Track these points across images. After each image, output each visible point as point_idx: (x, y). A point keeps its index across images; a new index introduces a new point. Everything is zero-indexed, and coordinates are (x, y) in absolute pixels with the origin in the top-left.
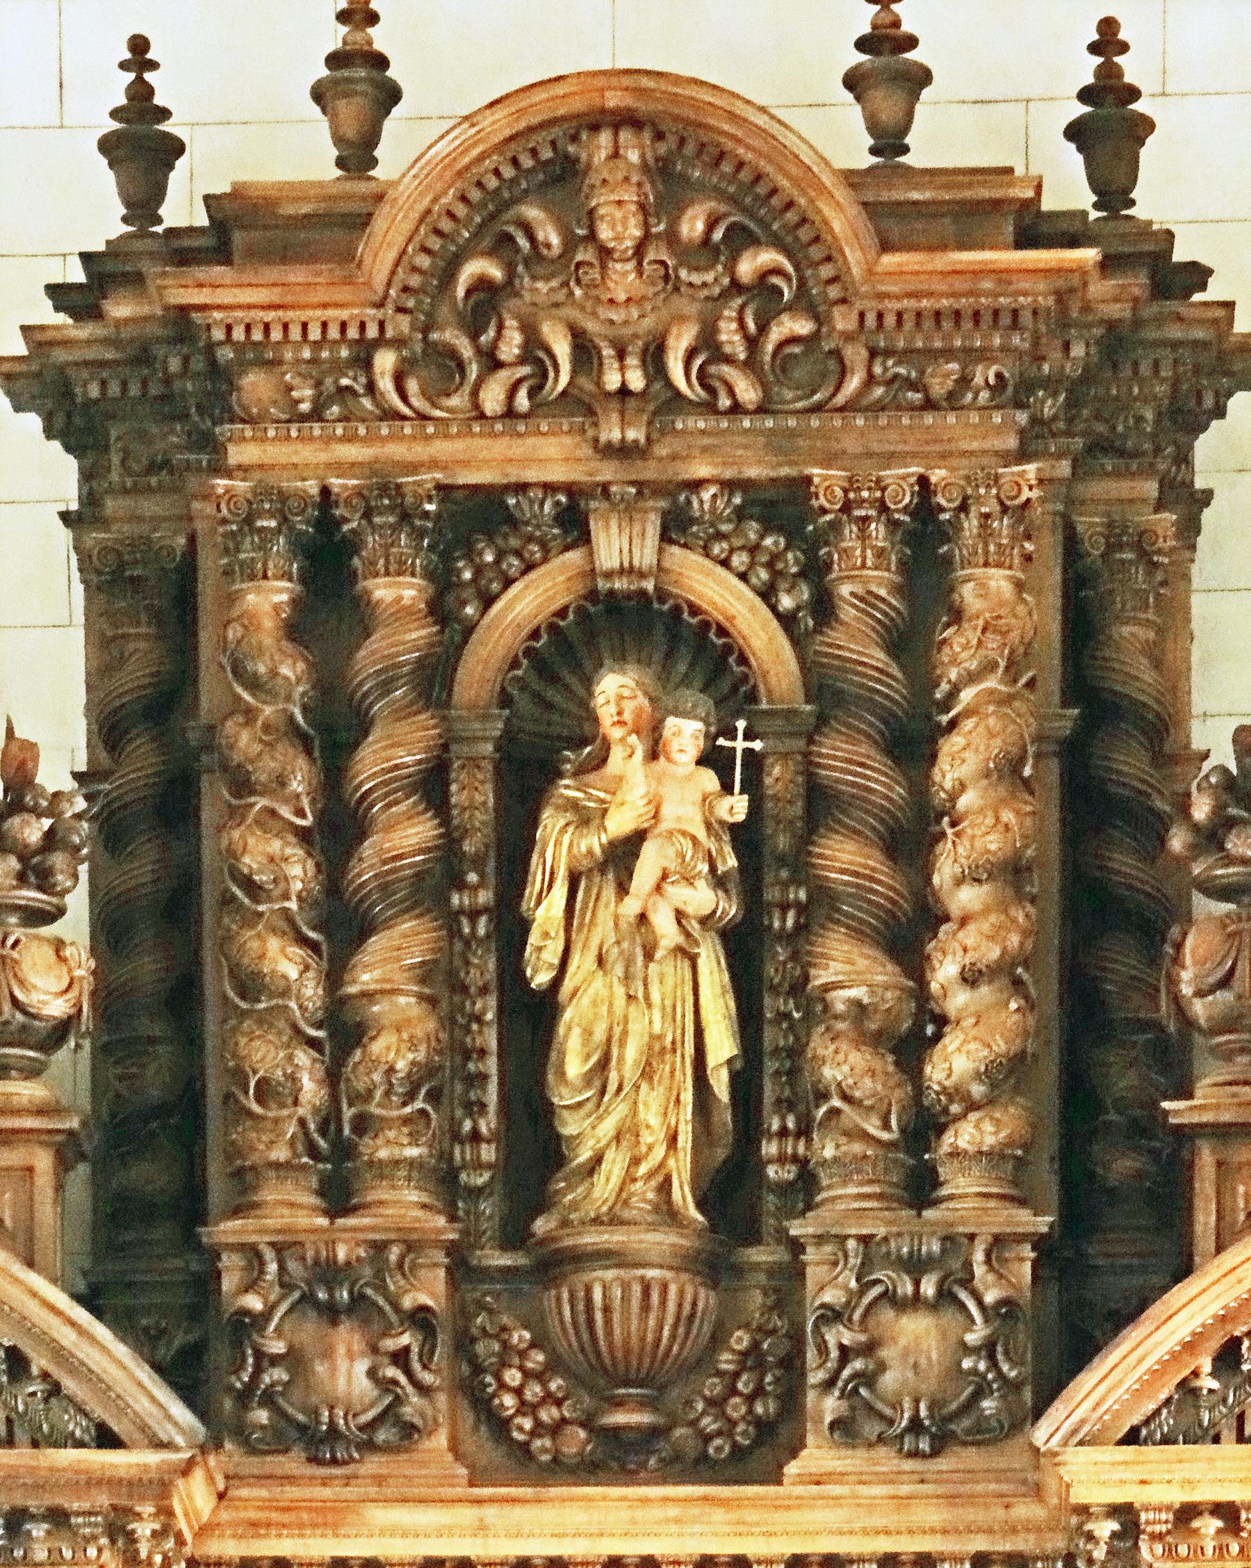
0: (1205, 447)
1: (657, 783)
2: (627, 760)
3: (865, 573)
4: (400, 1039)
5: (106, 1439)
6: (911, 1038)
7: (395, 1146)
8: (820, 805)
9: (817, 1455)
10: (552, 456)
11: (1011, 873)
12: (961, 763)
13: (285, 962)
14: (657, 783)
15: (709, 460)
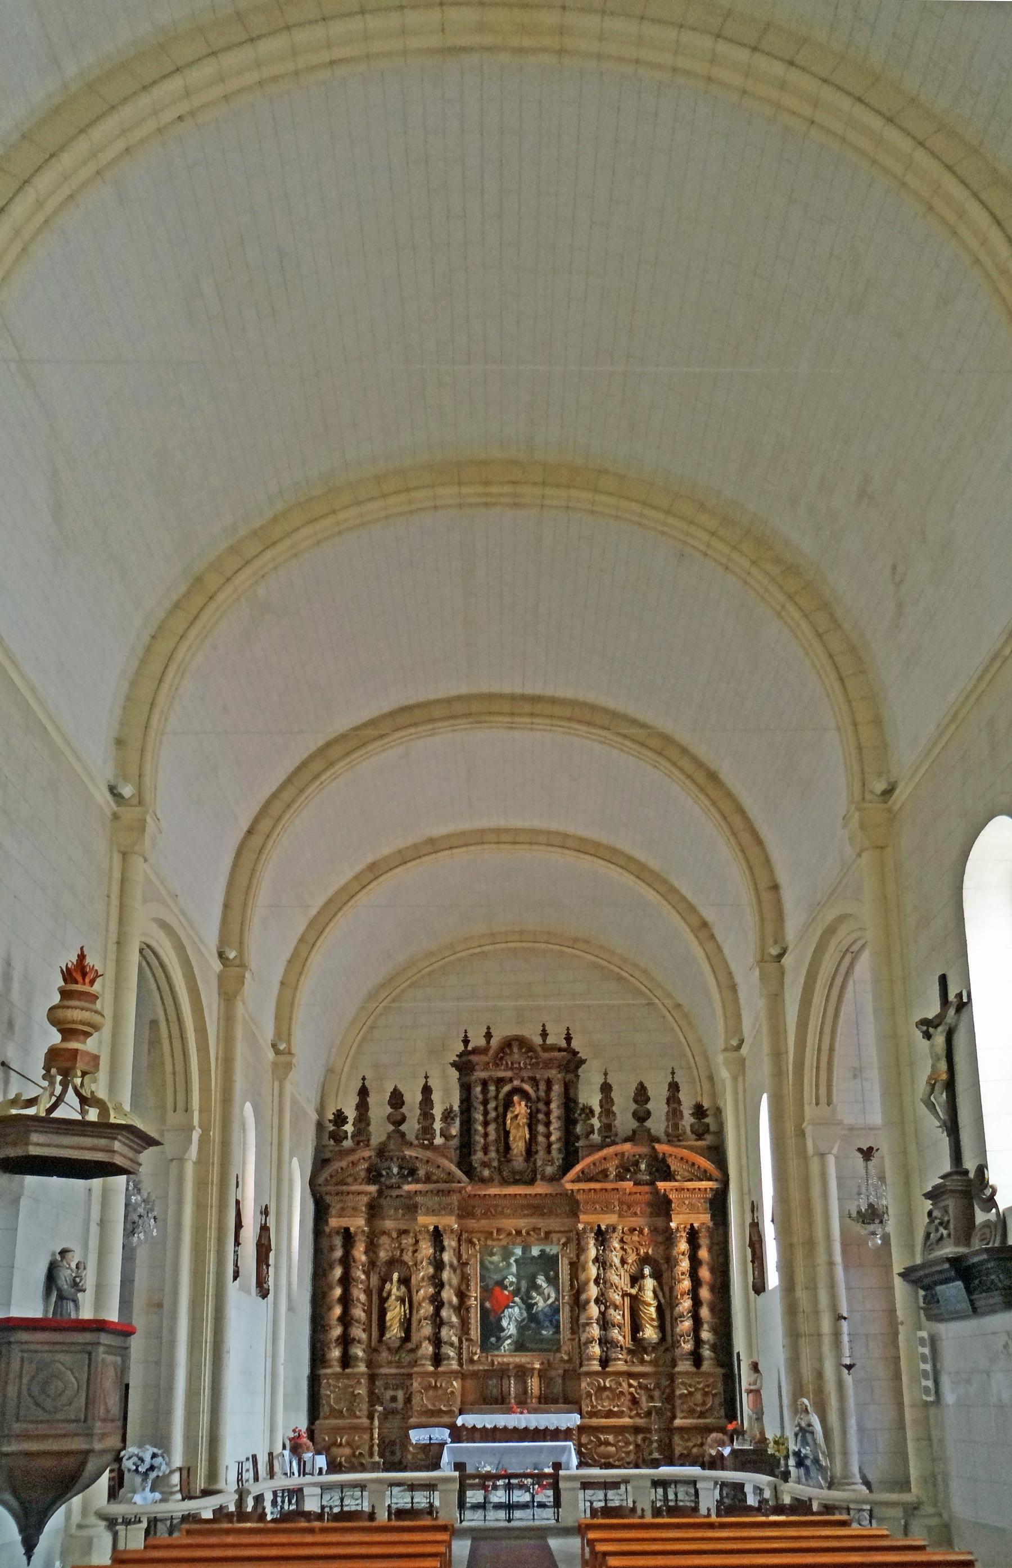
0: (580, 1070)
1: (521, 1108)
2: (517, 1106)
3: (542, 1086)
4: (492, 1137)
5: (459, 1182)
6: (548, 1136)
7: (492, 1148)
8: (538, 1111)
9: (539, 1182)
10: (509, 1074)
11: (559, 1118)
12: (553, 1106)
13: (480, 1128)
14: (521, 1108)
15: (525, 1074)
